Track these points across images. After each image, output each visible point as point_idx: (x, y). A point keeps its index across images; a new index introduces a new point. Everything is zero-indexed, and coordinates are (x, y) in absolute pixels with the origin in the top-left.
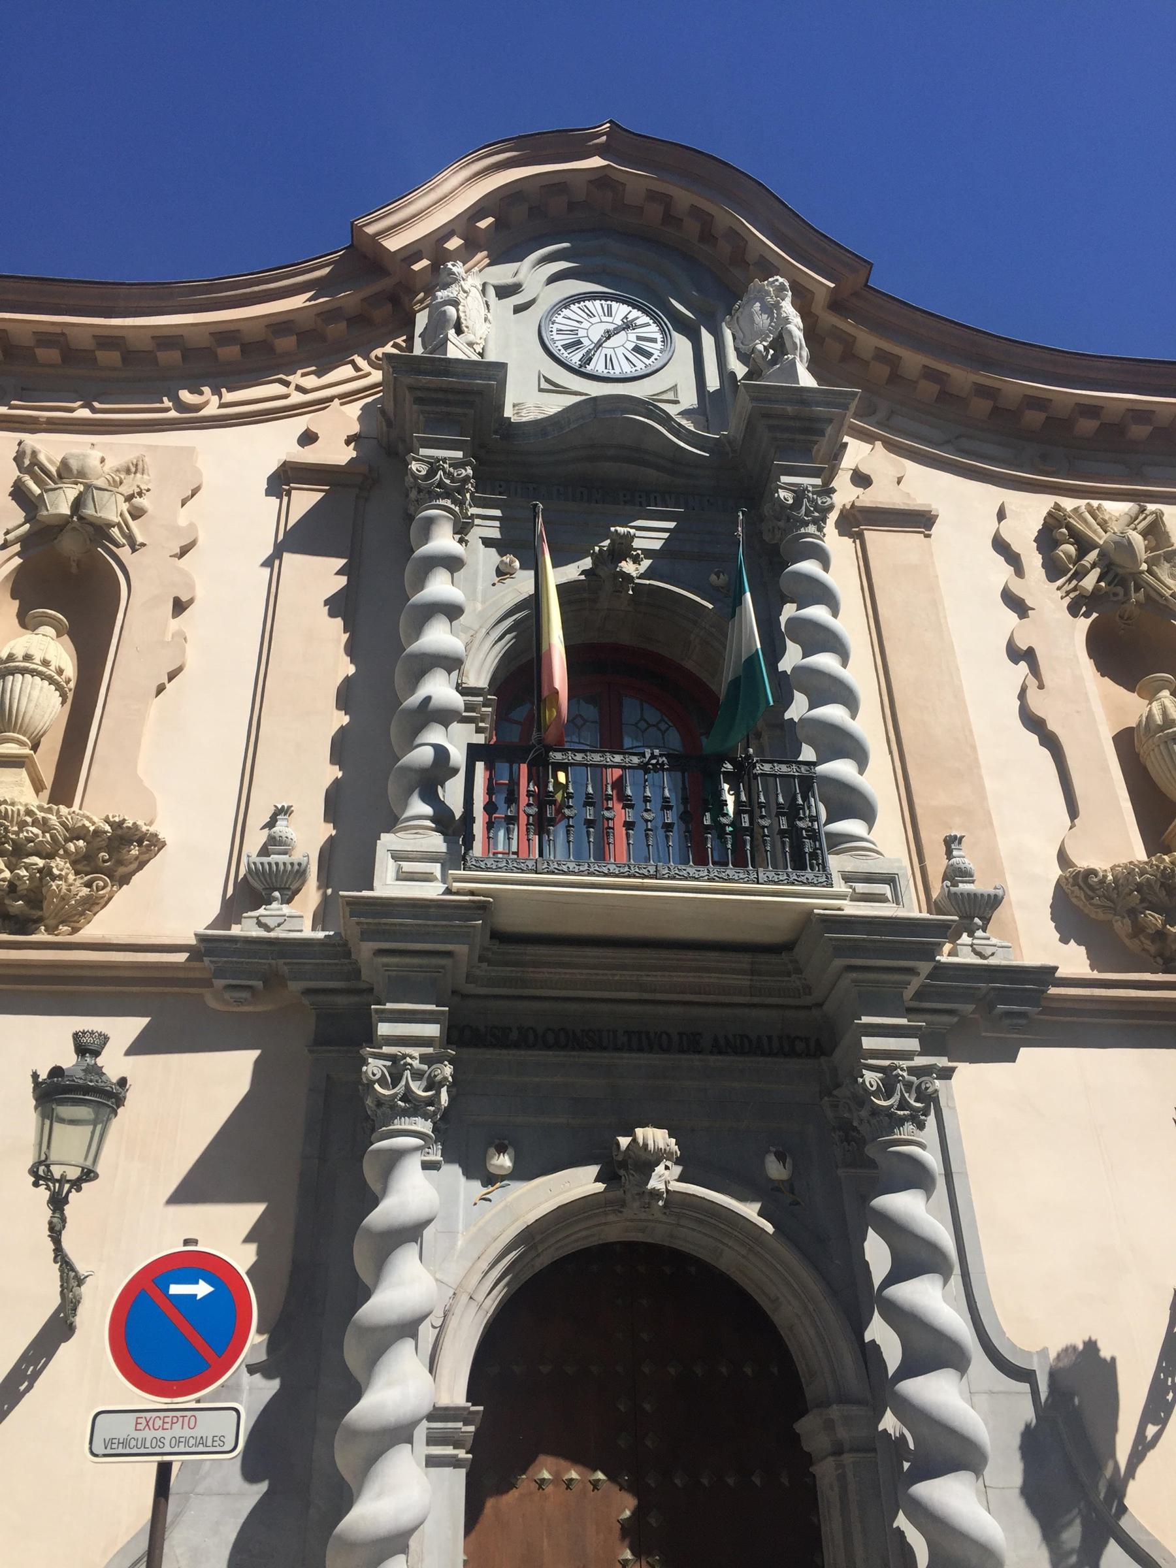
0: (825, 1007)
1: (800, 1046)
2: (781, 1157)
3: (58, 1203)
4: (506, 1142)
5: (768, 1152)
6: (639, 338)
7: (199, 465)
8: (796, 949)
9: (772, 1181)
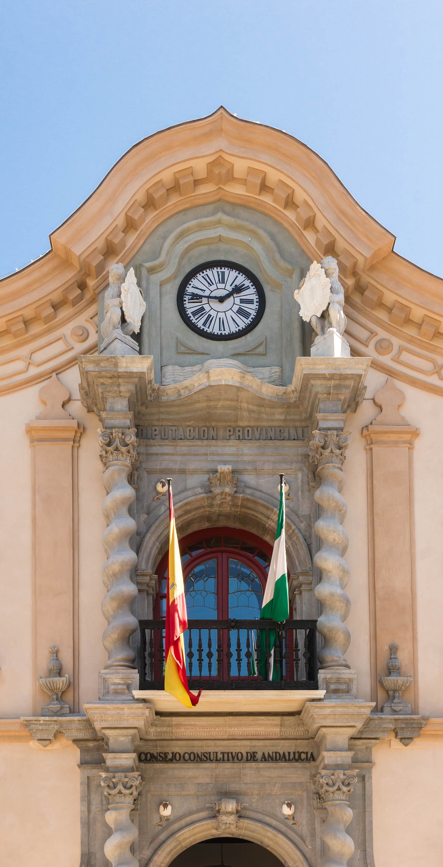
0: (315, 739)
1: (303, 756)
2: (289, 805)
3: (204, 598)
4: (168, 803)
5: (284, 803)
6: (242, 301)
7: (144, 303)
8: (302, 714)
9: (285, 815)
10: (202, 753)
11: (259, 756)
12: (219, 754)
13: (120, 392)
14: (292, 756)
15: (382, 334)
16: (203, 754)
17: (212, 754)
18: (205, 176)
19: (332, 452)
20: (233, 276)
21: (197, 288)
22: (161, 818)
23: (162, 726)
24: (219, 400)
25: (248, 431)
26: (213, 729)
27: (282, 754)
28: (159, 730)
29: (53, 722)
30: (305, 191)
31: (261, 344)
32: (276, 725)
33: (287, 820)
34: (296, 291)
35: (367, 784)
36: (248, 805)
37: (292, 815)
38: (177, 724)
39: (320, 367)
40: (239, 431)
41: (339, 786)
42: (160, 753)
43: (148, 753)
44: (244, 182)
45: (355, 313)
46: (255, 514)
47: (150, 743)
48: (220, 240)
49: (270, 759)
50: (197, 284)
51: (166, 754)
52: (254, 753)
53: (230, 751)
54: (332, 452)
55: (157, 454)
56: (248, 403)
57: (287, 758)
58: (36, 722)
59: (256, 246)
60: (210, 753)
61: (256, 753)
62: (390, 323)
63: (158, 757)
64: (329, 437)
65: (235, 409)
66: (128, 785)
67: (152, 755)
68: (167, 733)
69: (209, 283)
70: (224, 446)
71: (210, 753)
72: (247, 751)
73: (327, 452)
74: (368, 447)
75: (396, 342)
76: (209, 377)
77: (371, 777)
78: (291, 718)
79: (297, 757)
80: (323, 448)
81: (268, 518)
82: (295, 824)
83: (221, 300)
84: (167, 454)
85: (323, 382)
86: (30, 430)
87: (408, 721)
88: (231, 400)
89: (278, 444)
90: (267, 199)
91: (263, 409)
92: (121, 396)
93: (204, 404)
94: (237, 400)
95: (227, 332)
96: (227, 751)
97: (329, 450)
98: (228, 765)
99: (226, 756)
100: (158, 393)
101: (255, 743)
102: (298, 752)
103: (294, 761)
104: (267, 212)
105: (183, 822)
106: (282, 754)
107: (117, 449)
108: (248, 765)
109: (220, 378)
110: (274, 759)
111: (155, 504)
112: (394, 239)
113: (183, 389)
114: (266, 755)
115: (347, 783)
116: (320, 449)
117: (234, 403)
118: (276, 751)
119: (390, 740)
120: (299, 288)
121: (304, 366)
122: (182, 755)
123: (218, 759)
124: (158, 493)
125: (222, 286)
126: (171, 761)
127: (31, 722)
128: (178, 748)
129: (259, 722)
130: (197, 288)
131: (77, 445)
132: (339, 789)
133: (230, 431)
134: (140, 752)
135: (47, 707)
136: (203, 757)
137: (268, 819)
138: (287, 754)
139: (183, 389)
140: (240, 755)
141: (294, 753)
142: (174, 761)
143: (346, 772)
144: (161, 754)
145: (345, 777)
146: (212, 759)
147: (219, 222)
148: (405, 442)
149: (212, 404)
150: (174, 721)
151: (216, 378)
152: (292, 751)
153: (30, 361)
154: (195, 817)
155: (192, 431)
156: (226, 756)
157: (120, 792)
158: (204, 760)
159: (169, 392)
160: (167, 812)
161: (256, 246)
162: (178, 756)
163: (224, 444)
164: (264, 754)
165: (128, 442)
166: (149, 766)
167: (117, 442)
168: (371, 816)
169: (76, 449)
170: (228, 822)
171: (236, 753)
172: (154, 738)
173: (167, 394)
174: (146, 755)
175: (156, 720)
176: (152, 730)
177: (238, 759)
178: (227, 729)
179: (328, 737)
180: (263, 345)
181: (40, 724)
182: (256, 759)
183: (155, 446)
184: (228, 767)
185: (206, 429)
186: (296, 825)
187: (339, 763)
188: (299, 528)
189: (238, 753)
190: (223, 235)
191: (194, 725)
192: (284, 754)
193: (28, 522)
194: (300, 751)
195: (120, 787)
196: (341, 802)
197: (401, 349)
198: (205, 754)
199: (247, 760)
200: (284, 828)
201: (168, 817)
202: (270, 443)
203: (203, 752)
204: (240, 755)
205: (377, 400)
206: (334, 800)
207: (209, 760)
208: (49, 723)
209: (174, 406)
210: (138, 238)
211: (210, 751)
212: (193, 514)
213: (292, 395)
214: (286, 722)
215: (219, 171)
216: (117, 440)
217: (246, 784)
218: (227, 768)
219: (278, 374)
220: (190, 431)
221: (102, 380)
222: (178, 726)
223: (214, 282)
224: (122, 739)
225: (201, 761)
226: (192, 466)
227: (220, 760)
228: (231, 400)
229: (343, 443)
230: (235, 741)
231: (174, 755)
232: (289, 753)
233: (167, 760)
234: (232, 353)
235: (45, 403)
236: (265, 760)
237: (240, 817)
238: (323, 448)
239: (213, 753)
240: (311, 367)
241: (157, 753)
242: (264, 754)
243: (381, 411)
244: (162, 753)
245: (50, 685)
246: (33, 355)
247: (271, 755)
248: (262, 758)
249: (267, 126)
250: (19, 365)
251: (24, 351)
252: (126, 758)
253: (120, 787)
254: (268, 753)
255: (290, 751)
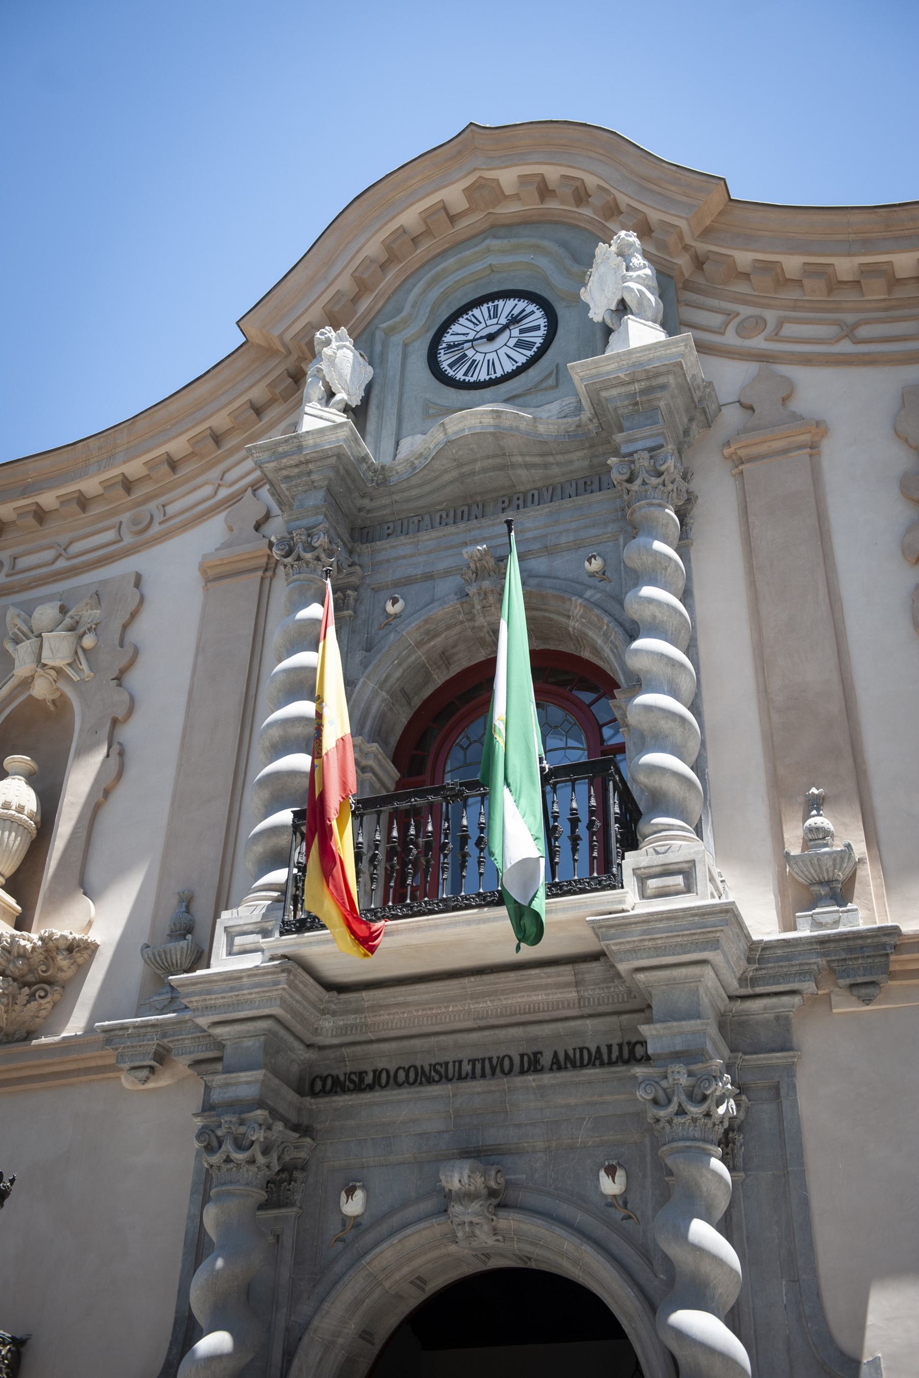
2: (611, 1172)
10: (430, 1065)
11: (546, 1060)
12: (465, 1063)
13: (313, 482)
14: (615, 1054)
15: (746, 311)
16: (433, 1067)
17: (451, 1066)
18: (467, 206)
19: (644, 483)
20: (508, 307)
21: (458, 334)
22: (345, 1219)
23: (346, 1012)
24: (475, 461)
25: (533, 495)
26: (443, 1010)
27: (593, 1051)
28: (341, 1023)
29: (149, 1029)
30: (594, 174)
31: (550, 374)
32: (567, 985)
33: (612, 1210)
34: (583, 290)
35: (786, 1103)
36: (524, 1176)
37: (622, 1195)
38: (373, 1006)
39: (608, 368)
40: (518, 499)
41: (680, 1105)
42: (351, 1073)
43: (327, 1076)
44: (516, 197)
45: (701, 297)
46: (547, 614)
47: (330, 1054)
48: (492, 271)
49: (569, 1065)
50: (461, 329)
51: (362, 1074)
52: (535, 1054)
53: (487, 1055)
54: (644, 483)
55: (388, 561)
56: (522, 455)
57: (605, 1057)
58: (121, 1033)
59: (543, 262)
60: (447, 1063)
61: (541, 1053)
62: (755, 293)
63: (347, 1083)
64: (637, 462)
65: (503, 467)
66: (246, 1143)
67: (336, 1080)
68: (356, 1028)
69: (474, 323)
70: (493, 525)
71: (447, 1063)
72: (521, 1052)
73: (636, 486)
74: (736, 470)
75: (771, 316)
76: (445, 430)
77: (794, 1087)
78: (594, 965)
79: (626, 1054)
80: (630, 480)
81: (569, 617)
82: (630, 1217)
83: (491, 338)
84: (404, 557)
85: (623, 390)
86: (203, 570)
87: (851, 943)
88: (494, 456)
89: (580, 502)
90: (552, 205)
91: (551, 459)
92: (315, 487)
93: (455, 474)
94: (504, 454)
95: (499, 373)
96: (481, 1056)
97: (638, 482)
98: (478, 1086)
99: (478, 1066)
100: (384, 475)
101: (534, 1030)
102: (629, 1043)
103: (620, 1063)
104: (555, 219)
105: (384, 1228)
106: (593, 1051)
107: (299, 558)
108: (519, 1081)
109: (461, 426)
110: (578, 1063)
111: (382, 633)
112: (722, 183)
113: (416, 459)
114: (561, 1057)
115: (699, 1097)
116: (626, 485)
117: (499, 461)
118: (581, 1045)
119: (829, 995)
120: (585, 285)
121: (582, 374)
122: (392, 1074)
123: (464, 1074)
124: (388, 616)
125: (495, 321)
126: (371, 1088)
127: (112, 1033)
128: (384, 1057)
129: (530, 982)
130: (458, 334)
131: (269, 574)
132: (681, 1112)
133: (503, 502)
134: (314, 1075)
135: (147, 1001)
136: (433, 1073)
137: (565, 1209)
138: (604, 1050)
139: (416, 459)
140: (507, 1062)
141: (620, 1046)
142: (377, 1087)
143: (693, 1067)
144: (353, 1077)
145: (692, 1081)
146: (450, 1075)
147: (488, 250)
148: (800, 447)
149: (465, 469)
150: (366, 998)
151: (456, 429)
152: (614, 1042)
153: (221, 482)
154: (410, 1212)
155: (444, 516)
156: (478, 1066)
157: (228, 1160)
158: (434, 1081)
159: (399, 468)
160: (354, 1206)
161: (543, 262)
162: (384, 1075)
163: (490, 522)
164: (556, 1054)
165: (316, 545)
166: (323, 1103)
167: (299, 549)
168: (804, 1186)
169: (267, 582)
170: (467, 1219)
171: (498, 1058)
172: (336, 1041)
173: (397, 473)
174: (324, 1080)
175: (329, 1002)
176: (327, 1023)
177: (502, 1071)
178: (472, 1006)
179: (654, 992)
180: (554, 376)
181: (129, 1036)
182: (539, 1068)
183: (385, 549)
184: (479, 1090)
185: (466, 509)
186: (630, 1221)
187: (678, 1048)
188: (620, 620)
189: (504, 1057)
190: (494, 263)
191: (406, 1004)
192: (598, 1048)
193: (184, 698)
194: (634, 1040)
195: (228, 1146)
196: (688, 1144)
197: (780, 324)
198: (438, 1067)
199: (522, 1072)
200: (601, 1231)
201: (359, 1220)
202: (567, 503)
203: (433, 1062)
204: (507, 1062)
205: (743, 401)
206: (673, 1140)
207: (444, 1080)
208: (143, 1030)
209: (411, 488)
210: (376, 300)
211: (447, 1059)
212: (443, 636)
213: (591, 427)
214: (587, 977)
215: (483, 193)
216: (300, 545)
217: (519, 1126)
218: (478, 1093)
219: (575, 405)
220: (441, 517)
221: (284, 473)
222: (375, 1008)
223: (482, 320)
224: (248, 1043)
225: (430, 1081)
226: (442, 566)
227: (466, 1078)
228: (494, 456)
229: (662, 465)
230: (491, 1032)
231: (377, 1074)
232: (610, 1047)
233: (363, 1086)
234: (506, 397)
235: (231, 529)
236: (560, 1069)
237: (501, 1206)
238: (630, 480)
239: (454, 1062)
240: (594, 371)
241: (345, 1074)
242: (556, 1054)
243: (754, 411)
244: (355, 1073)
245: (161, 960)
246: (226, 475)
247: (571, 1055)
248: (553, 1063)
249: (531, 123)
250: (207, 490)
251: (215, 473)
252: (248, 1083)
253: (228, 1146)
254: (566, 1051)
255: (610, 1042)
